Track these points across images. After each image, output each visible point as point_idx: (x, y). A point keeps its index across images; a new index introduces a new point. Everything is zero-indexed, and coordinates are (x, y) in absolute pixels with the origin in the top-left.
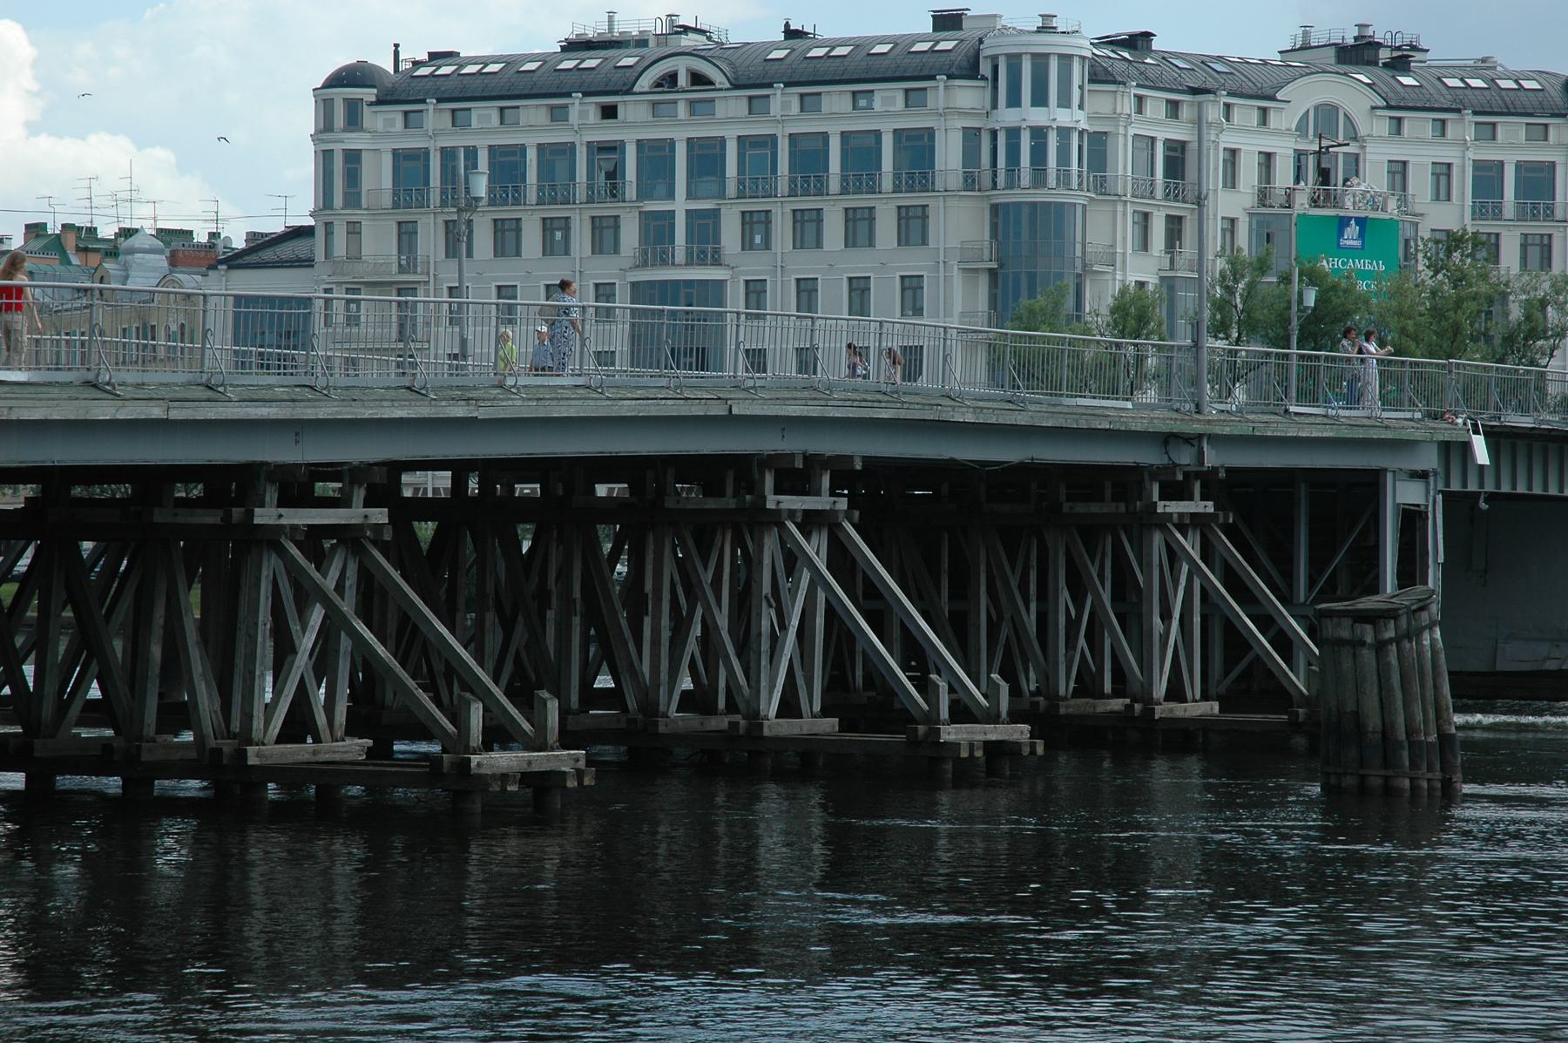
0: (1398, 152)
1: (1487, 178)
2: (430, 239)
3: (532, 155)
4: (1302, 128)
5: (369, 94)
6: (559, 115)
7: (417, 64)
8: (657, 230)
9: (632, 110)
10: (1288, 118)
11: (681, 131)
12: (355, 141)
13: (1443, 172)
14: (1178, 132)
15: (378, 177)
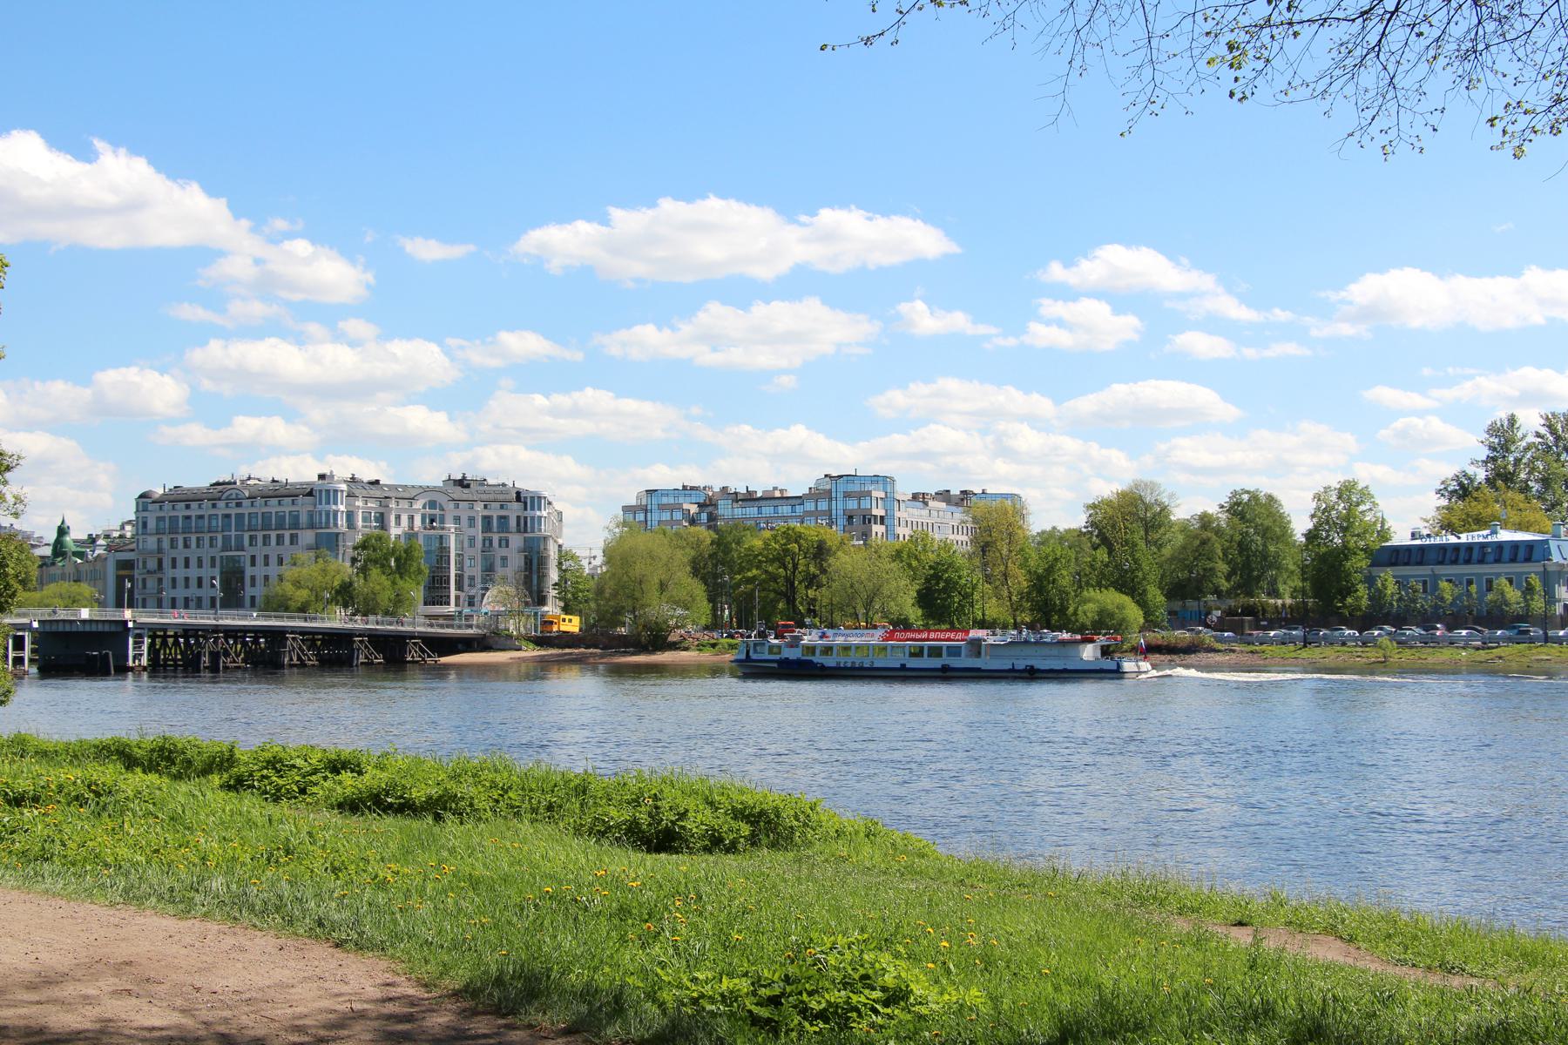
0: (457, 513)
1: (487, 520)
2: (166, 544)
3: (193, 518)
4: (424, 507)
5: (150, 500)
6: (188, 507)
7: (170, 490)
8: (226, 539)
10: (418, 505)
11: (233, 511)
12: (145, 514)
13: (472, 520)
14: (381, 510)
15: (152, 524)
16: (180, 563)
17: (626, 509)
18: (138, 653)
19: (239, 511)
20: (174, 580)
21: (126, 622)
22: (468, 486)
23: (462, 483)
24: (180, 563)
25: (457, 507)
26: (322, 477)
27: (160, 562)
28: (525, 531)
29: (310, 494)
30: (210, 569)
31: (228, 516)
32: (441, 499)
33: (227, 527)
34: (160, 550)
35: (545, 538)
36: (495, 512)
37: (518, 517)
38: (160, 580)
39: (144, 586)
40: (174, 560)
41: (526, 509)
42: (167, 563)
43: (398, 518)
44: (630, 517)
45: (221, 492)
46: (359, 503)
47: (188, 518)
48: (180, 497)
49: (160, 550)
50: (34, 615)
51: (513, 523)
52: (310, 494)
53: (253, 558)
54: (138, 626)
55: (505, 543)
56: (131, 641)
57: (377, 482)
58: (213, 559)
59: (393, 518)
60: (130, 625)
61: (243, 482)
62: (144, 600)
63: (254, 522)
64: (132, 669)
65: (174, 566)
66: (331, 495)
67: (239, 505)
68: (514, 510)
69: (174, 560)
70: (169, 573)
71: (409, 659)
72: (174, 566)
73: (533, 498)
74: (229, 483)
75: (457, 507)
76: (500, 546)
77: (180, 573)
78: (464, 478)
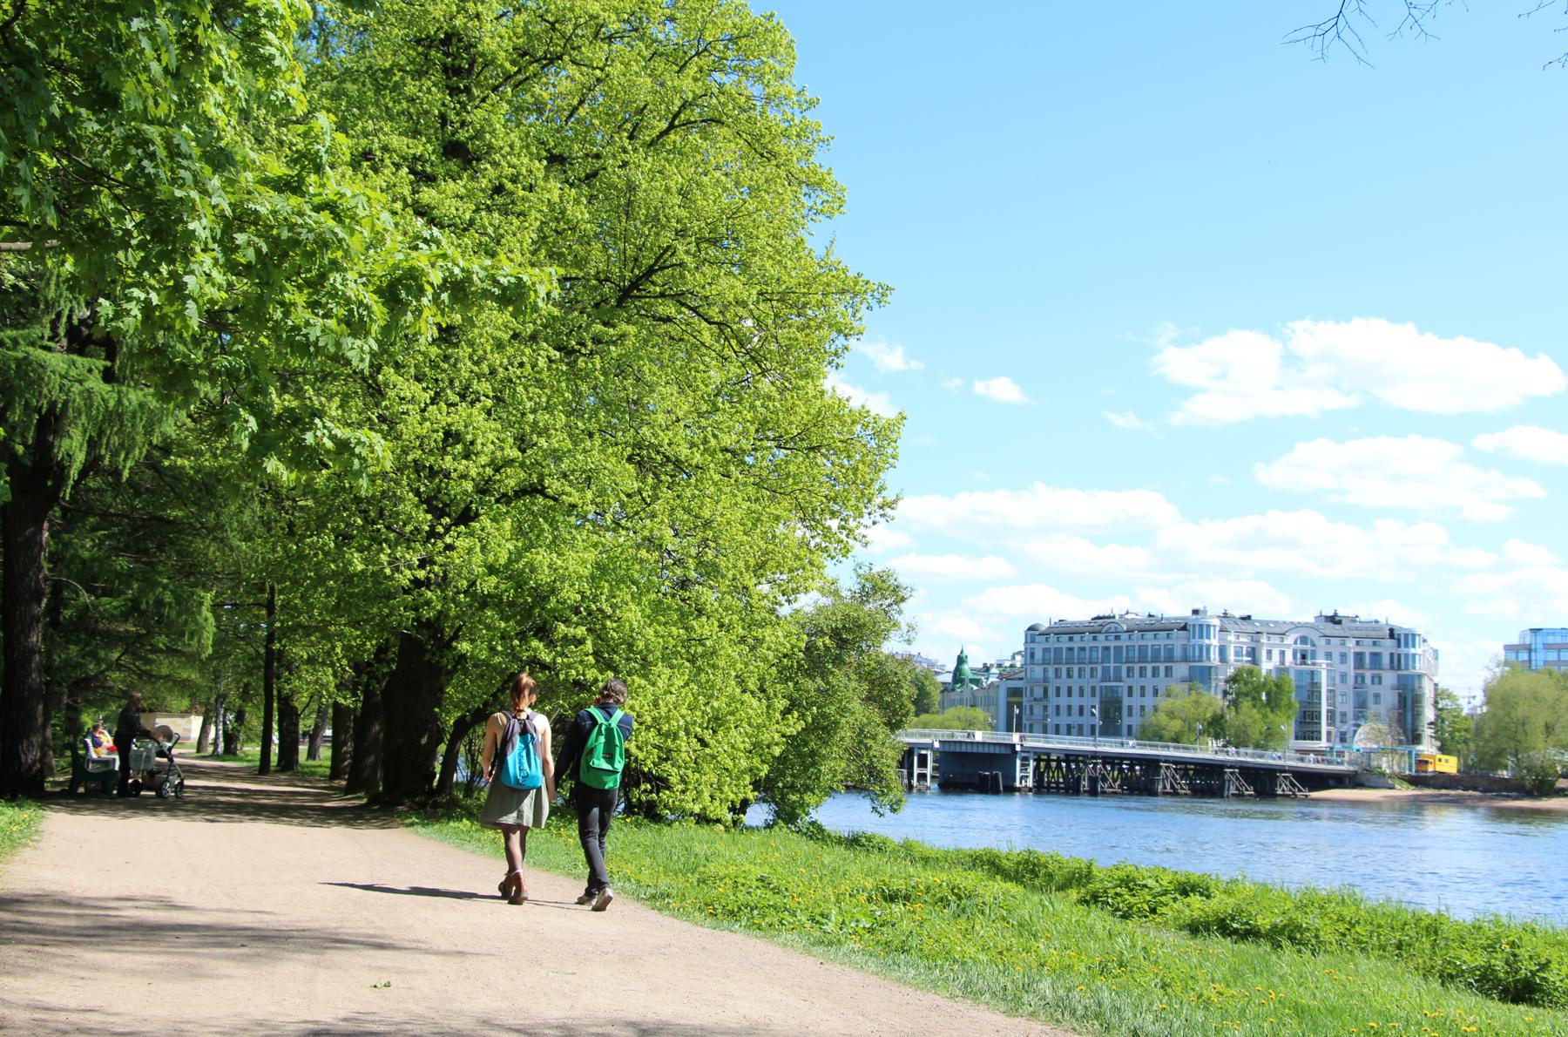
1: (1359, 657)
2: (1051, 674)
4: (1295, 643)
6: (1071, 639)
9: (1101, 637)
10: (1290, 640)
11: (1112, 644)
12: (1032, 645)
15: (1039, 655)
16: (1064, 691)
17: (1508, 648)
18: (1024, 775)
19: (1118, 643)
20: (1058, 707)
21: (1014, 746)
22: (1339, 622)
23: (1334, 620)
24: (1064, 691)
25: (1328, 643)
26: (1195, 612)
27: (1046, 690)
28: (1399, 669)
29: (1184, 628)
30: (1140, 698)
31: (1107, 649)
32: (1313, 635)
33: (1105, 659)
34: (1046, 680)
35: (1420, 676)
36: (1367, 649)
37: (1392, 654)
38: (1045, 708)
39: (1031, 713)
40: (1058, 689)
41: (1399, 646)
42: (1052, 691)
43: (1269, 652)
44: (1512, 656)
45: (1102, 625)
46: (1231, 637)
47: (1071, 649)
48: (1065, 631)
49: (1046, 680)
50: (936, 736)
51: (1386, 660)
52: (1184, 628)
53: (1130, 688)
54: (1025, 750)
55: (1377, 680)
56: (1018, 762)
57: (1249, 617)
58: (1093, 689)
59: (1264, 653)
60: (1018, 748)
61: (1121, 616)
62: (1031, 726)
63: (1131, 654)
64: (1019, 790)
65: (1058, 695)
66: (1204, 630)
67: (1117, 638)
68: (1387, 647)
69: (1058, 689)
70: (1053, 701)
71: (1279, 792)
72: (1058, 695)
73: (1406, 636)
74: (1109, 617)
75: (1328, 643)
76: (1373, 683)
77: (1063, 701)
78: (1336, 615)
